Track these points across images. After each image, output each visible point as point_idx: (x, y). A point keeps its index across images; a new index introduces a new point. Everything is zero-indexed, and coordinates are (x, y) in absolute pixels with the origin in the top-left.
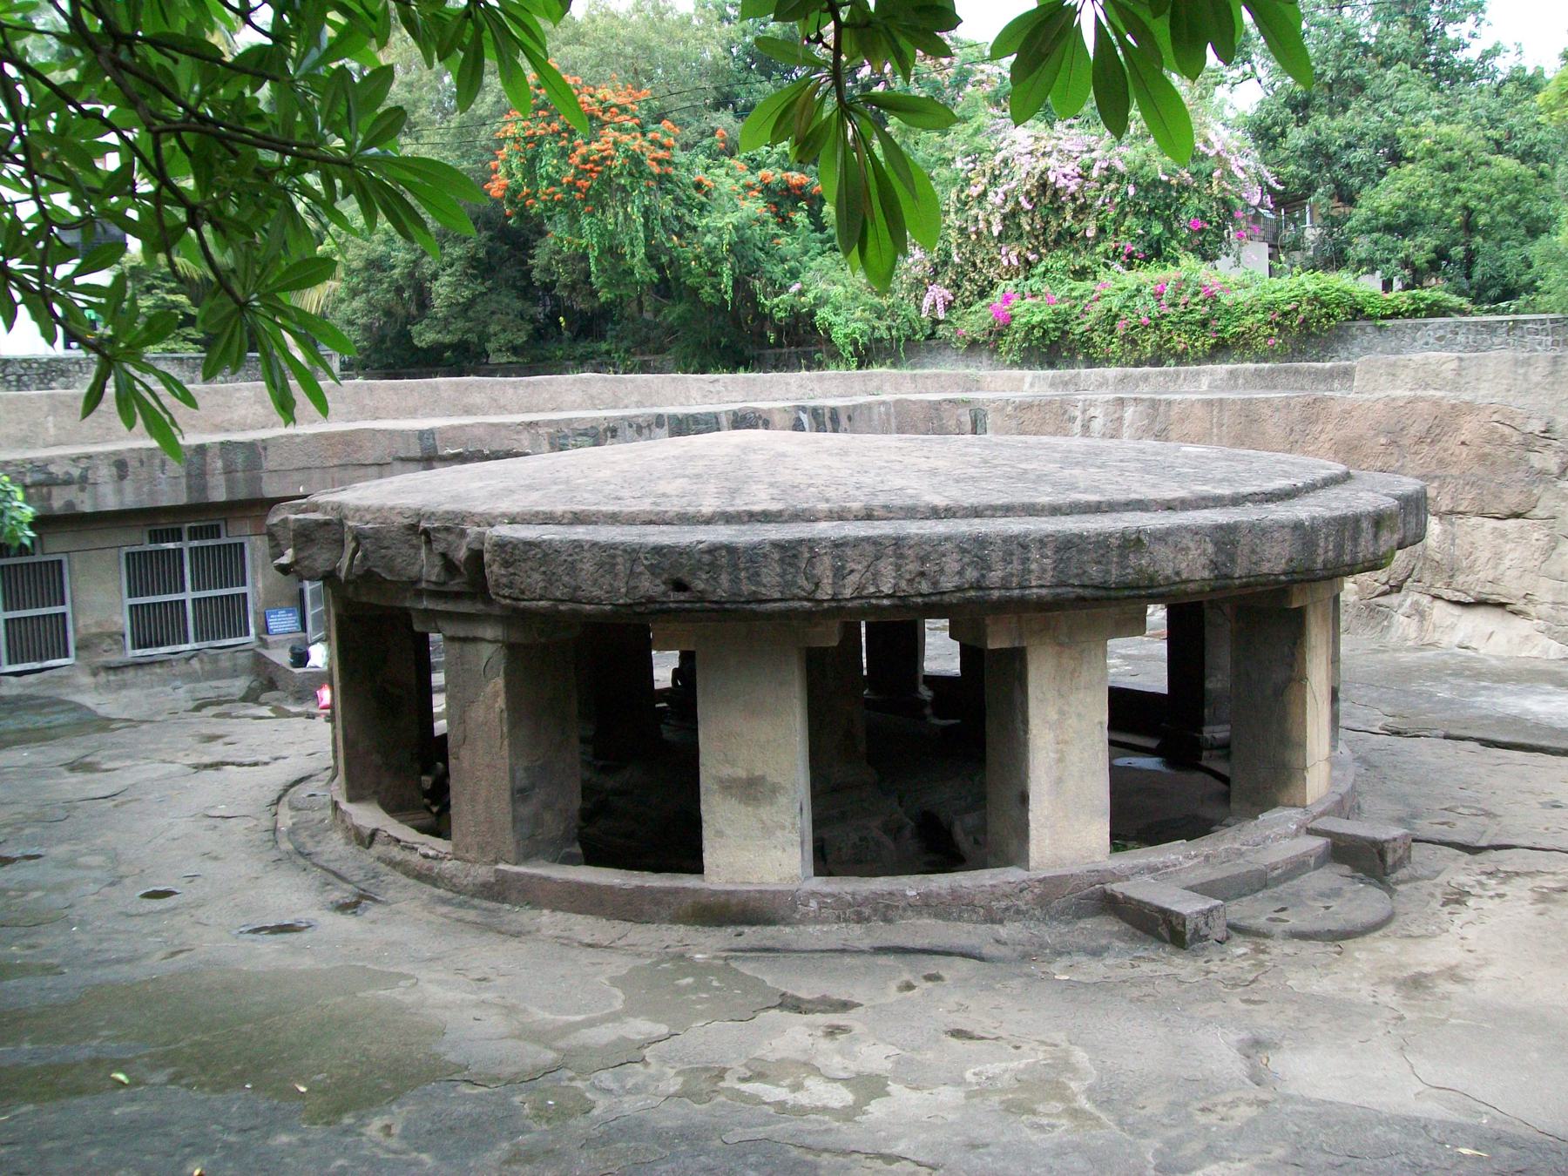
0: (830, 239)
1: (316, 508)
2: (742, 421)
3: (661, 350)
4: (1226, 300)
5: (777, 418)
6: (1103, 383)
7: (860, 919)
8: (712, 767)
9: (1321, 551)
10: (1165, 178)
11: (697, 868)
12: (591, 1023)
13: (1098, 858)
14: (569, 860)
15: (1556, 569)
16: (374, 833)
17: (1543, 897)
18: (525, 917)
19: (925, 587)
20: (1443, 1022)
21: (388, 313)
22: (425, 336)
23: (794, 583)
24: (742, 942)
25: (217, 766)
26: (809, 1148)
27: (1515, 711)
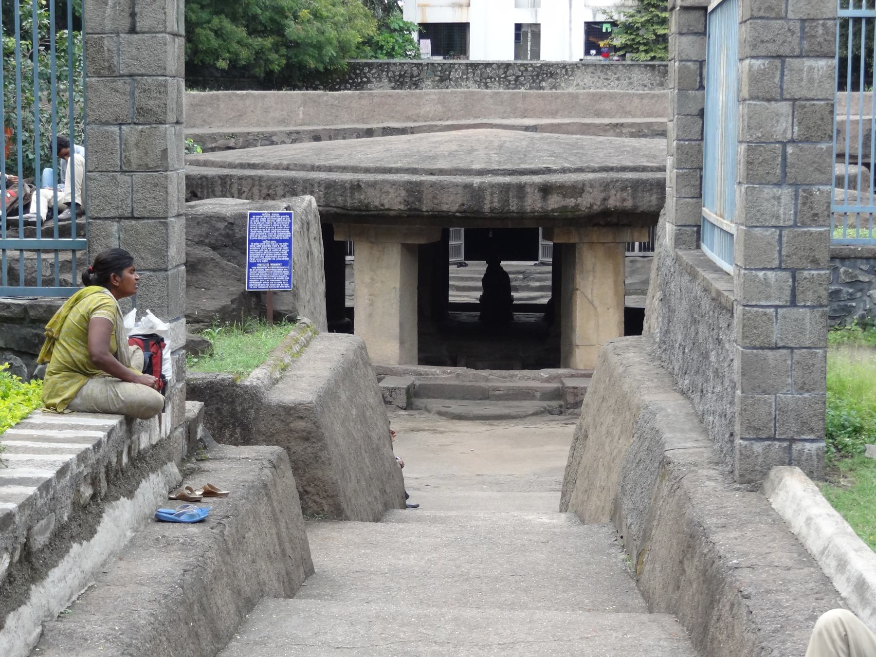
9: (487, 202)
13: (392, 362)
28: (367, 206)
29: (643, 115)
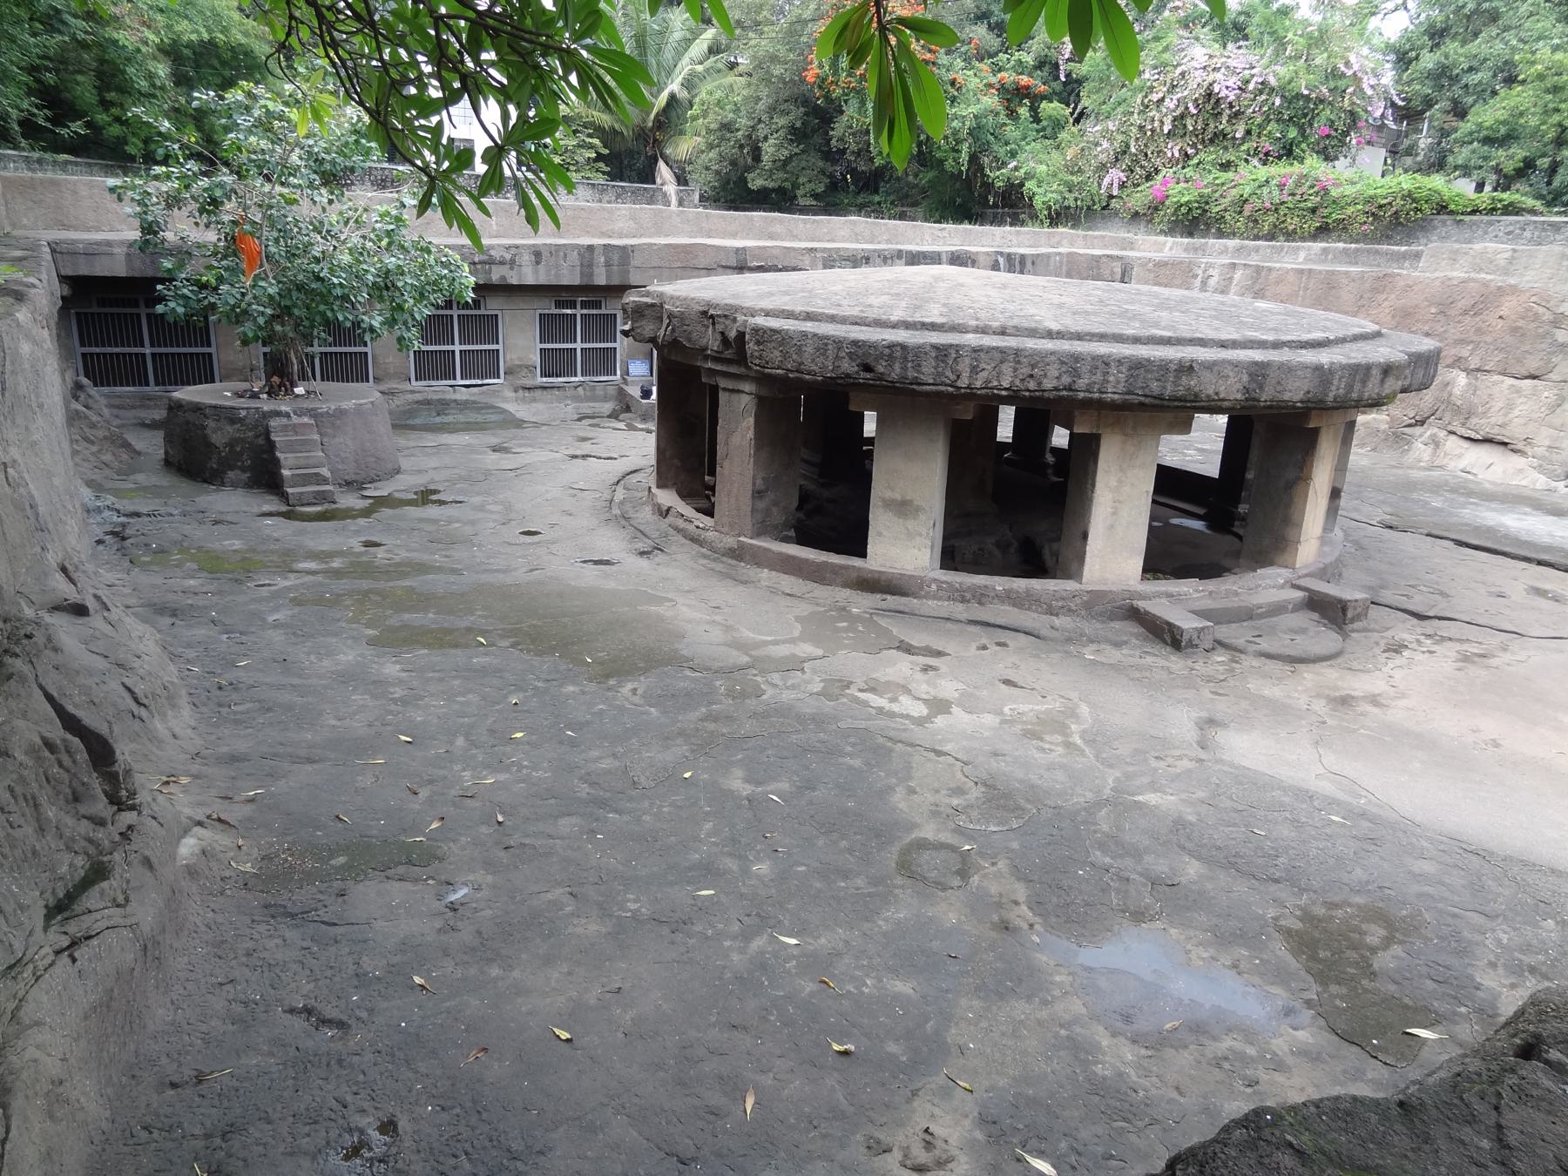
0: (1044, 129)
1: (648, 294)
2: (957, 259)
3: (915, 204)
4: (1334, 193)
5: (981, 259)
6: (1225, 251)
7: (963, 600)
8: (880, 490)
10: (1306, 92)
11: (863, 554)
12: (776, 643)
14: (786, 540)
15: (1557, 421)
16: (669, 510)
17: (1466, 658)
18: (751, 572)
19: (1032, 385)
20: (1354, 731)
21: (733, 163)
22: (756, 182)
23: (943, 374)
24: (884, 605)
25: (584, 457)
26: (890, 739)
27: (1491, 523)
28: (1196, 395)
29: (807, 240)
